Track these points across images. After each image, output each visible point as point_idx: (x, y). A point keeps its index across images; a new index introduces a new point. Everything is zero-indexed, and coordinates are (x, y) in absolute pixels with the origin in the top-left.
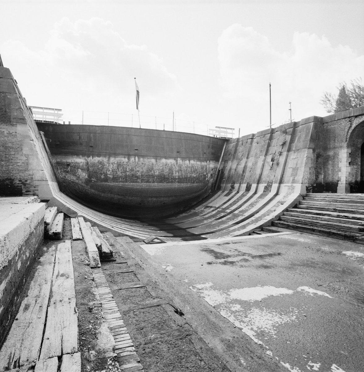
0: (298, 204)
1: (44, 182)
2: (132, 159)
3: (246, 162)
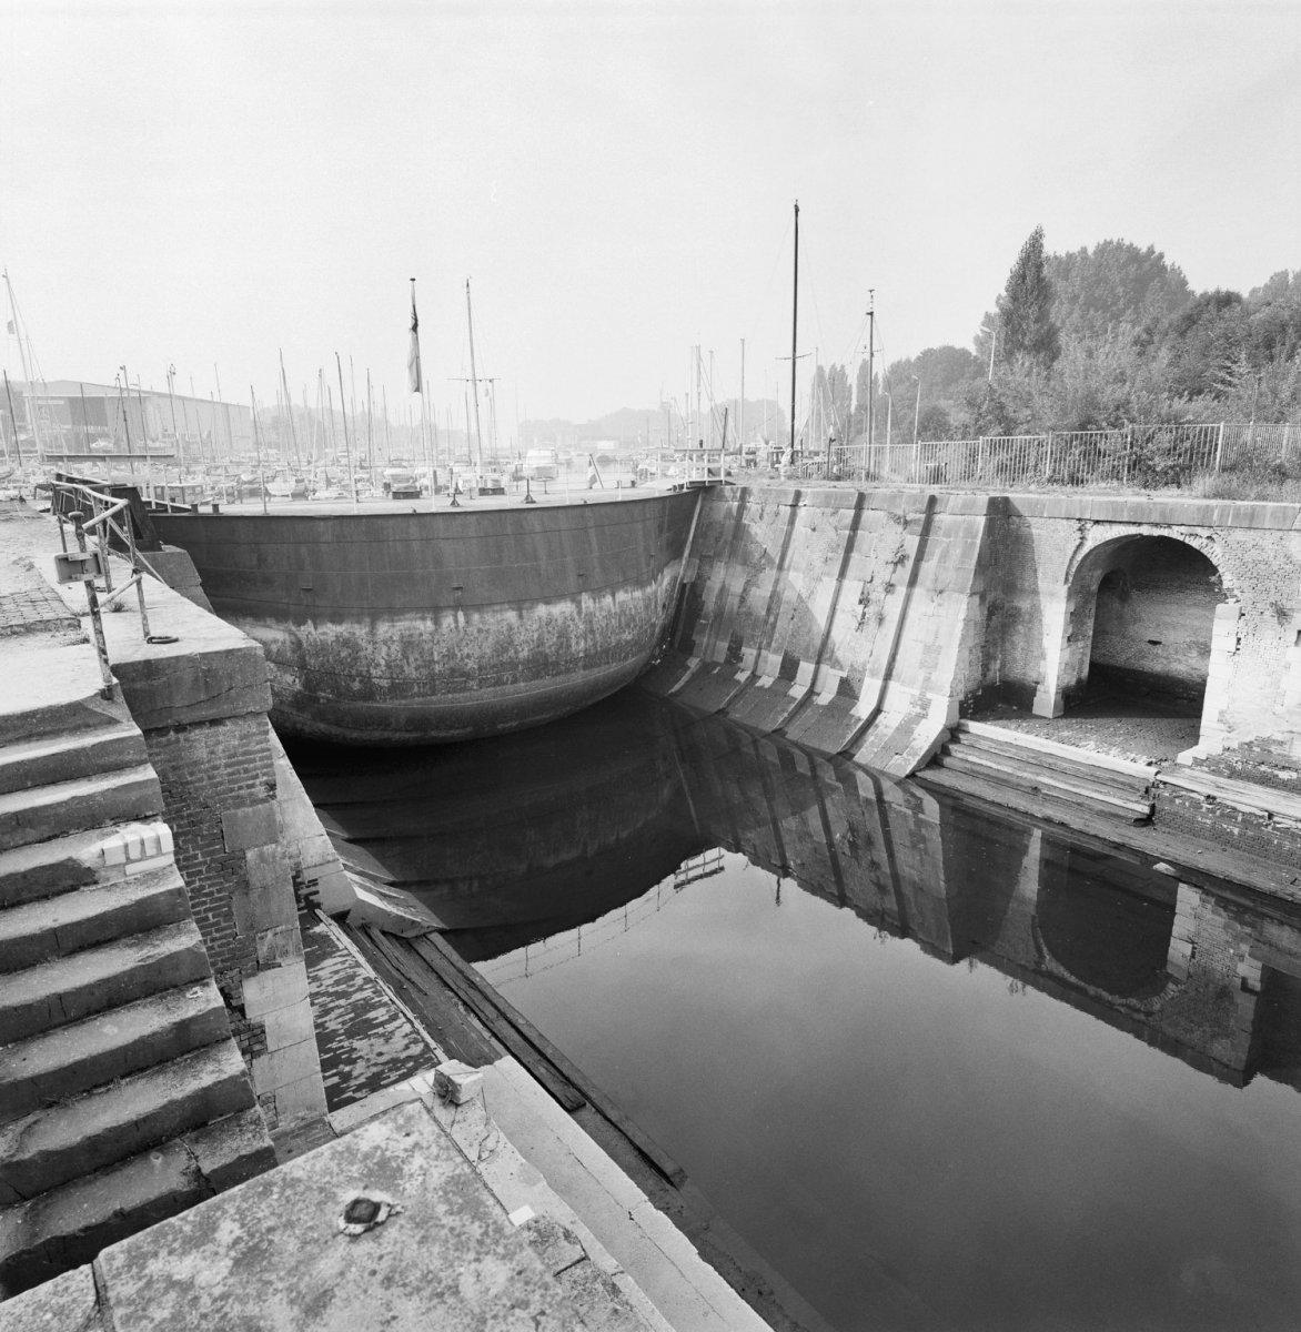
1: (331, 865)
2: (448, 621)
3: (777, 581)
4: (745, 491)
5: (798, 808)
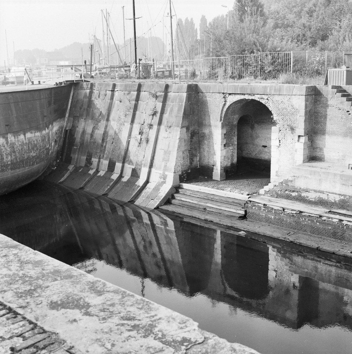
0: (170, 198)
3: (106, 126)
4: (92, 85)
5: (122, 233)
